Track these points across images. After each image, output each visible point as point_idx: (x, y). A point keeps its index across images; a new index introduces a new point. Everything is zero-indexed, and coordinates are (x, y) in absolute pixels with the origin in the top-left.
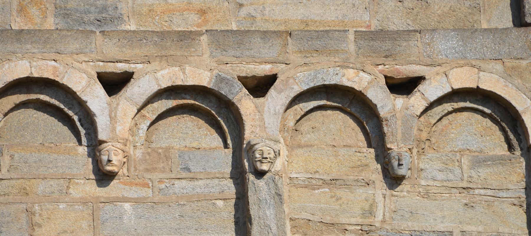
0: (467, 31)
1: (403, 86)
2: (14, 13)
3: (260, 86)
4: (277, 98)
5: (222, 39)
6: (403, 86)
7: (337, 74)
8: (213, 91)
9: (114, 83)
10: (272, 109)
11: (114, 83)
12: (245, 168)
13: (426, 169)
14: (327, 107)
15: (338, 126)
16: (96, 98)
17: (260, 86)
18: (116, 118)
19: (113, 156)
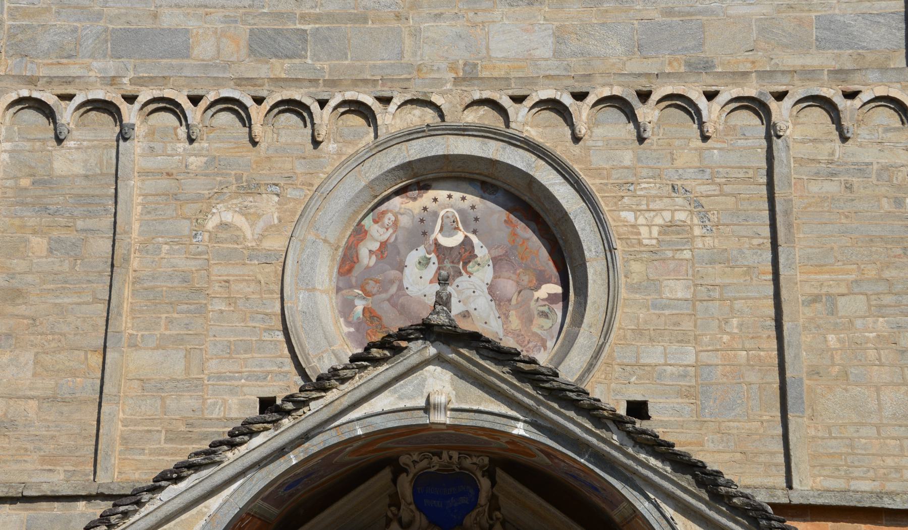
0: (883, 69)
4: (788, 102)
5: (763, 75)
6: (851, 95)
12: (771, 134)
13: (861, 134)
15: (818, 115)
16: (702, 103)
18: (711, 111)
19: (710, 128)
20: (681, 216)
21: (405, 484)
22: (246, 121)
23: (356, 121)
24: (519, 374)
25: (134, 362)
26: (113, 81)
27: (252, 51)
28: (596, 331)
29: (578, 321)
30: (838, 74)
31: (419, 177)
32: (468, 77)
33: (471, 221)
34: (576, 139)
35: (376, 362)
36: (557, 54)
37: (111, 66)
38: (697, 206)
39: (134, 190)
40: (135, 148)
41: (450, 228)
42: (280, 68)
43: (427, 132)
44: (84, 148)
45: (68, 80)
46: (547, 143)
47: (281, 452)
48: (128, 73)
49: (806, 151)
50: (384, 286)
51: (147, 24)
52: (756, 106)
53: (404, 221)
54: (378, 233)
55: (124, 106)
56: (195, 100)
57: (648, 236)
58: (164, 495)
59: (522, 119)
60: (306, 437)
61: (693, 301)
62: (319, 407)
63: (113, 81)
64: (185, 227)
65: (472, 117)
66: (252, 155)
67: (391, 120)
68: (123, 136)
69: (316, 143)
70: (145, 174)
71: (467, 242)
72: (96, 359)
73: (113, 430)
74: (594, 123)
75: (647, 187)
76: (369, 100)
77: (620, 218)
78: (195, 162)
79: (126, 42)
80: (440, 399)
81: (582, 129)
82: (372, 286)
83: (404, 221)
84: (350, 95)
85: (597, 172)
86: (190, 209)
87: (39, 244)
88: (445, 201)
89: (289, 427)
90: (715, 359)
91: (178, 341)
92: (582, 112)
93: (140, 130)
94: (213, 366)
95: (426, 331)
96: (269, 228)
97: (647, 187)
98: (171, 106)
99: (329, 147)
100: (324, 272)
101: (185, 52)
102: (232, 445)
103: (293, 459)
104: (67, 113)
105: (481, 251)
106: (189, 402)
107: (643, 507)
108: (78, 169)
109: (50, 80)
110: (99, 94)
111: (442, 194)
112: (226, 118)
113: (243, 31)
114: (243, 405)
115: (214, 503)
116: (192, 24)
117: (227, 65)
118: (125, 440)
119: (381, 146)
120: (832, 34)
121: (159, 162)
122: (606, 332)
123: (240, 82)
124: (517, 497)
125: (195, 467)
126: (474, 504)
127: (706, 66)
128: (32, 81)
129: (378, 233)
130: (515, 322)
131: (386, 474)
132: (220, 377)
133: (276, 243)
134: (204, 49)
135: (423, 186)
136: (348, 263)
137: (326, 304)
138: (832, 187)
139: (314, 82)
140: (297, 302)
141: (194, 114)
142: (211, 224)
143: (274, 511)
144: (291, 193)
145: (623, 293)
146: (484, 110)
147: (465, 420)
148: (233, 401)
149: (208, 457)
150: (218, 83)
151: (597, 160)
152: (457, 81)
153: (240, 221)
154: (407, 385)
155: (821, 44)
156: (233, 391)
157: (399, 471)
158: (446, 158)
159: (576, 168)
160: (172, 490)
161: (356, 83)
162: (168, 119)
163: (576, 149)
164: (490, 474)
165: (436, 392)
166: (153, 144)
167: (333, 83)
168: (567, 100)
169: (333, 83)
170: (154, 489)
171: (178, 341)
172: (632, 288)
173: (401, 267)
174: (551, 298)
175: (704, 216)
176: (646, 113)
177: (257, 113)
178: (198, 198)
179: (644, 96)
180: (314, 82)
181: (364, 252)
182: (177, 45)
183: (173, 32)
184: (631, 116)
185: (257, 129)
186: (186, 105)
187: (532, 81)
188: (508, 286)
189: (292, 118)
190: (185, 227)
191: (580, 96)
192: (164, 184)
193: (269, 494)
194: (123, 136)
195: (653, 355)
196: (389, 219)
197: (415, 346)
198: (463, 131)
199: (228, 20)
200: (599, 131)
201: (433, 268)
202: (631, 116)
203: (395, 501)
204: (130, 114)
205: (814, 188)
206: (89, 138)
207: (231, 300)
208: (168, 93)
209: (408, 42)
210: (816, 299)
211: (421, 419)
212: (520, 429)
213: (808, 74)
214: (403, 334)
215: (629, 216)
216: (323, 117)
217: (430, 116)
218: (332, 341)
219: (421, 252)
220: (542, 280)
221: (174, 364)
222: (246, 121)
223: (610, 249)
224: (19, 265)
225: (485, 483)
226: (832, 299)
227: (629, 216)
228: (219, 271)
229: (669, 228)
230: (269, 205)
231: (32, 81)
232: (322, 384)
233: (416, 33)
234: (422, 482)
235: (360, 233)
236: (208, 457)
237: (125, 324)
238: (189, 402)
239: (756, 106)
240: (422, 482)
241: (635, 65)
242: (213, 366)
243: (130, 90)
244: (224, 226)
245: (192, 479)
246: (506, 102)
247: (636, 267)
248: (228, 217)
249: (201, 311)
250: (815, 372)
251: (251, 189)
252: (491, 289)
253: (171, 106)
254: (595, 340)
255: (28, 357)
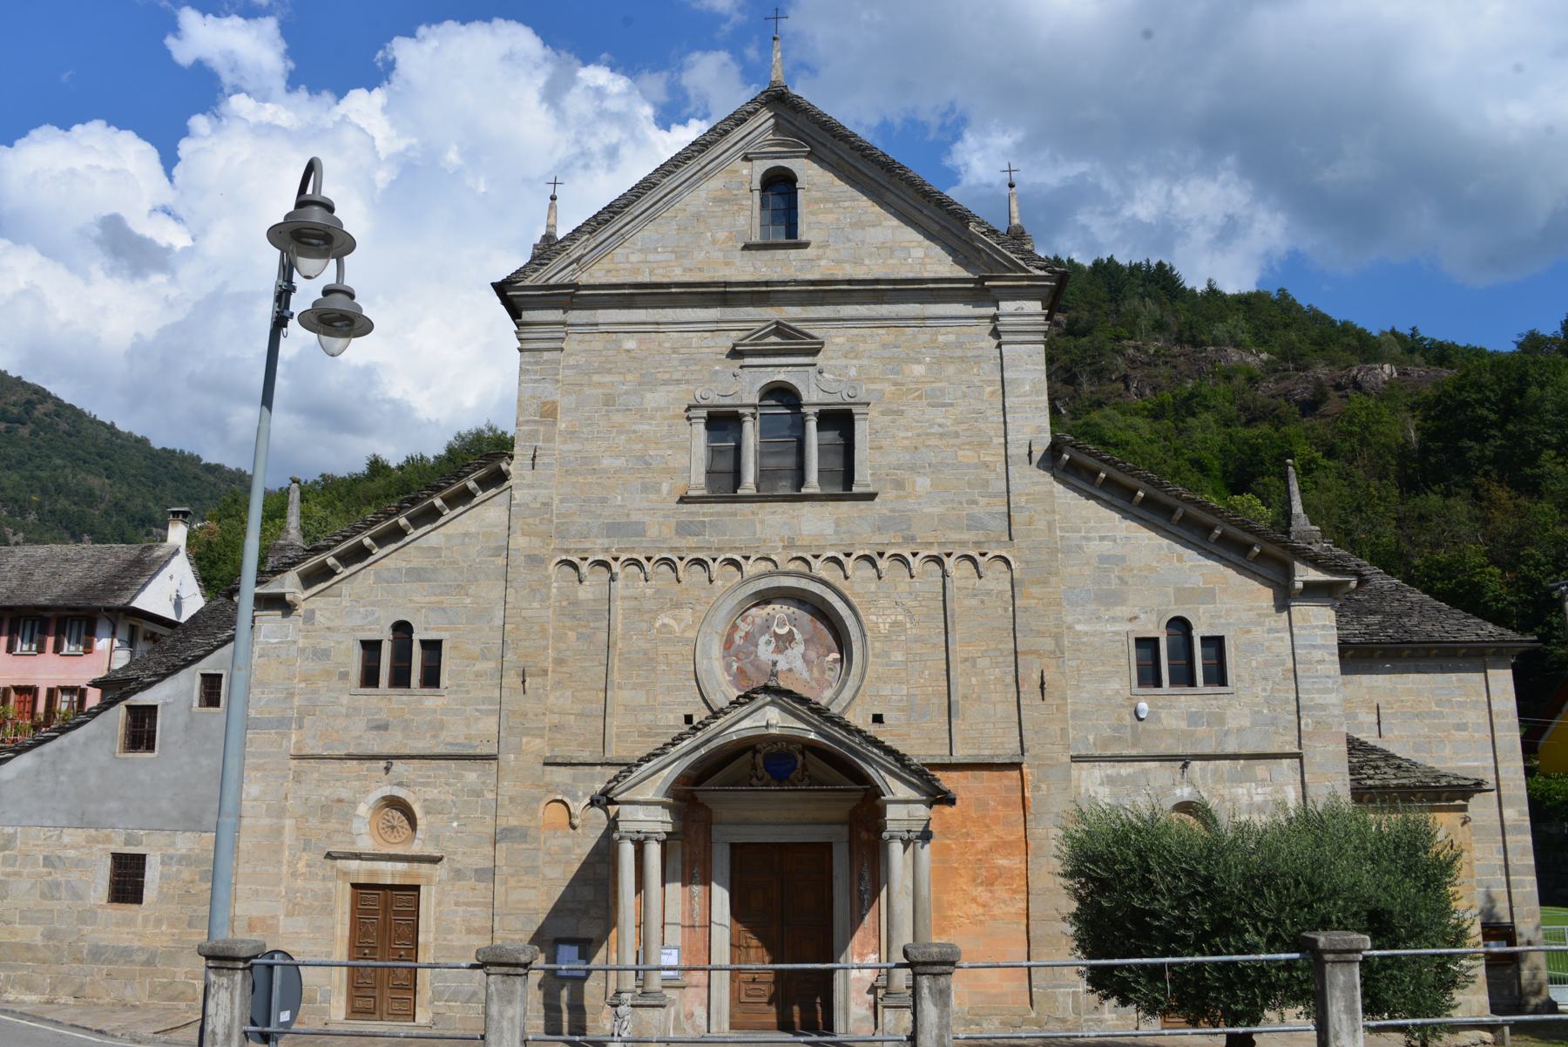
0: (998, 542)
1: (983, 555)
2: (1516, 949)
3: (949, 555)
4: (953, 558)
5: (940, 544)
6: (983, 555)
7: (393, 827)
8: (882, 868)
9: (914, 555)
10: (1381, 429)
11: (914, 555)
12: (945, 575)
13: (988, 574)
14: (792, 598)
15: (968, 564)
16: (910, 558)
17: (949, 555)
18: (915, 563)
19: (914, 572)
20: (900, 618)
21: (760, 759)
22: (675, 569)
23: (732, 569)
24: (811, 709)
25: (621, 696)
26: (607, 550)
27: (677, 533)
28: (857, 679)
29: (848, 672)
30: (977, 544)
31: (764, 598)
32: (790, 545)
33: (793, 621)
34: (846, 578)
35: (742, 704)
36: (836, 532)
37: (606, 542)
38: (908, 611)
39: (618, 606)
40: (619, 585)
41: (781, 624)
42: (692, 541)
43: (769, 574)
44: (592, 586)
45: (585, 550)
46: (831, 580)
47: (697, 748)
48: (615, 544)
49: (962, 583)
50: (748, 655)
51: (624, 520)
52: (937, 560)
53: (758, 621)
54: (744, 627)
55: (613, 563)
56: (649, 559)
57: (884, 628)
58: (642, 768)
59: (819, 568)
60: (709, 741)
61: (906, 662)
62: (714, 726)
63: (607, 550)
64: (644, 626)
65: (792, 566)
66: (677, 587)
67: (750, 568)
68: (612, 579)
69: (711, 581)
70: (624, 598)
71: (791, 631)
72: (602, 695)
73: (612, 731)
74: (855, 569)
75: (883, 602)
76: (738, 558)
77: (869, 619)
78: (649, 592)
79: (613, 529)
80: (773, 722)
81: (849, 573)
82: (741, 656)
83: (758, 621)
84: (728, 555)
85: (857, 595)
86: (646, 617)
87: (572, 635)
88: (779, 610)
89: (701, 736)
90: (917, 692)
91: (642, 685)
92: (849, 563)
93: (621, 576)
94: (660, 698)
95: (766, 689)
96: (688, 626)
97: (883, 602)
98: (637, 563)
99: (718, 583)
100: (716, 649)
101: (642, 534)
102: (674, 745)
103: (703, 751)
104: (584, 568)
105: (798, 636)
106: (649, 717)
107: (870, 771)
108: (590, 596)
109: (576, 551)
110: (600, 557)
111: (777, 607)
112: (665, 568)
113: (673, 521)
114: (676, 718)
115: (666, 772)
116: (646, 519)
117: (665, 540)
118: (618, 736)
119: (745, 582)
120: (974, 523)
121: (630, 592)
122: (862, 679)
123: (671, 549)
124: (818, 766)
125: (656, 755)
126: (795, 768)
127: (913, 539)
128: (567, 551)
129: (744, 627)
130: (816, 673)
131: (749, 754)
132: (664, 704)
133: (691, 634)
134: (653, 532)
135: (768, 603)
136: (728, 643)
137: (718, 665)
138: (974, 602)
139: (709, 549)
140: (702, 665)
141: (648, 566)
142: (657, 625)
143: (694, 773)
144: (698, 608)
145: (871, 658)
146: (798, 562)
147: (786, 732)
148: (671, 716)
149: (663, 750)
150: (660, 550)
151: (857, 589)
152: (784, 547)
153: (672, 622)
154: (757, 715)
155: (969, 528)
156: (670, 711)
157: (756, 751)
158: (779, 588)
159: (847, 593)
160: (646, 766)
161: (732, 549)
162: (635, 569)
163: (847, 583)
164: (803, 754)
165: (772, 719)
166: (627, 583)
167: (719, 549)
168: (842, 557)
169: (719, 549)
170: (638, 766)
171: (642, 685)
172: (876, 656)
173: (756, 645)
174: (835, 661)
175: (912, 618)
176: (883, 564)
177: (680, 565)
178: (650, 611)
179: (881, 555)
180: (709, 549)
181: (737, 637)
182: (638, 530)
183: (637, 523)
184: (874, 565)
185: (681, 574)
186: (644, 562)
187: (823, 547)
188: (812, 655)
189: (699, 568)
190: (644, 626)
191: (848, 555)
192: (633, 603)
193: (692, 767)
194: (612, 579)
195: (886, 691)
196: (749, 620)
197: (761, 696)
198: (787, 574)
199: (665, 516)
200: (858, 573)
201: (773, 645)
202: (874, 565)
203: (754, 767)
204: (616, 567)
205: (966, 602)
206: (595, 580)
207: (668, 664)
208: (635, 556)
209: (758, 526)
210: (966, 660)
211: (765, 732)
212: (812, 736)
213: (963, 544)
214: (755, 691)
215: (874, 618)
216: (715, 567)
217: (770, 566)
218: (724, 690)
219: (767, 637)
220: (830, 651)
221: (641, 697)
222: (675, 569)
223: (864, 636)
224: (562, 646)
225: (800, 758)
226: (974, 660)
227: (874, 618)
228: (662, 649)
229: (894, 624)
230: (687, 614)
231: (567, 551)
232: (715, 715)
233: (762, 522)
234: (767, 757)
235: (735, 627)
236: (663, 750)
237: (615, 676)
238: (649, 717)
239: (937, 560)
240: (767, 757)
241: (877, 539)
242: (660, 698)
243: (616, 554)
244: (664, 625)
245: (655, 761)
246: (810, 558)
247: (877, 645)
248: (666, 621)
249: (654, 670)
250: (965, 697)
251: (678, 605)
252: (803, 656)
253: (637, 563)
254: (857, 683)
255: (568, 693)
